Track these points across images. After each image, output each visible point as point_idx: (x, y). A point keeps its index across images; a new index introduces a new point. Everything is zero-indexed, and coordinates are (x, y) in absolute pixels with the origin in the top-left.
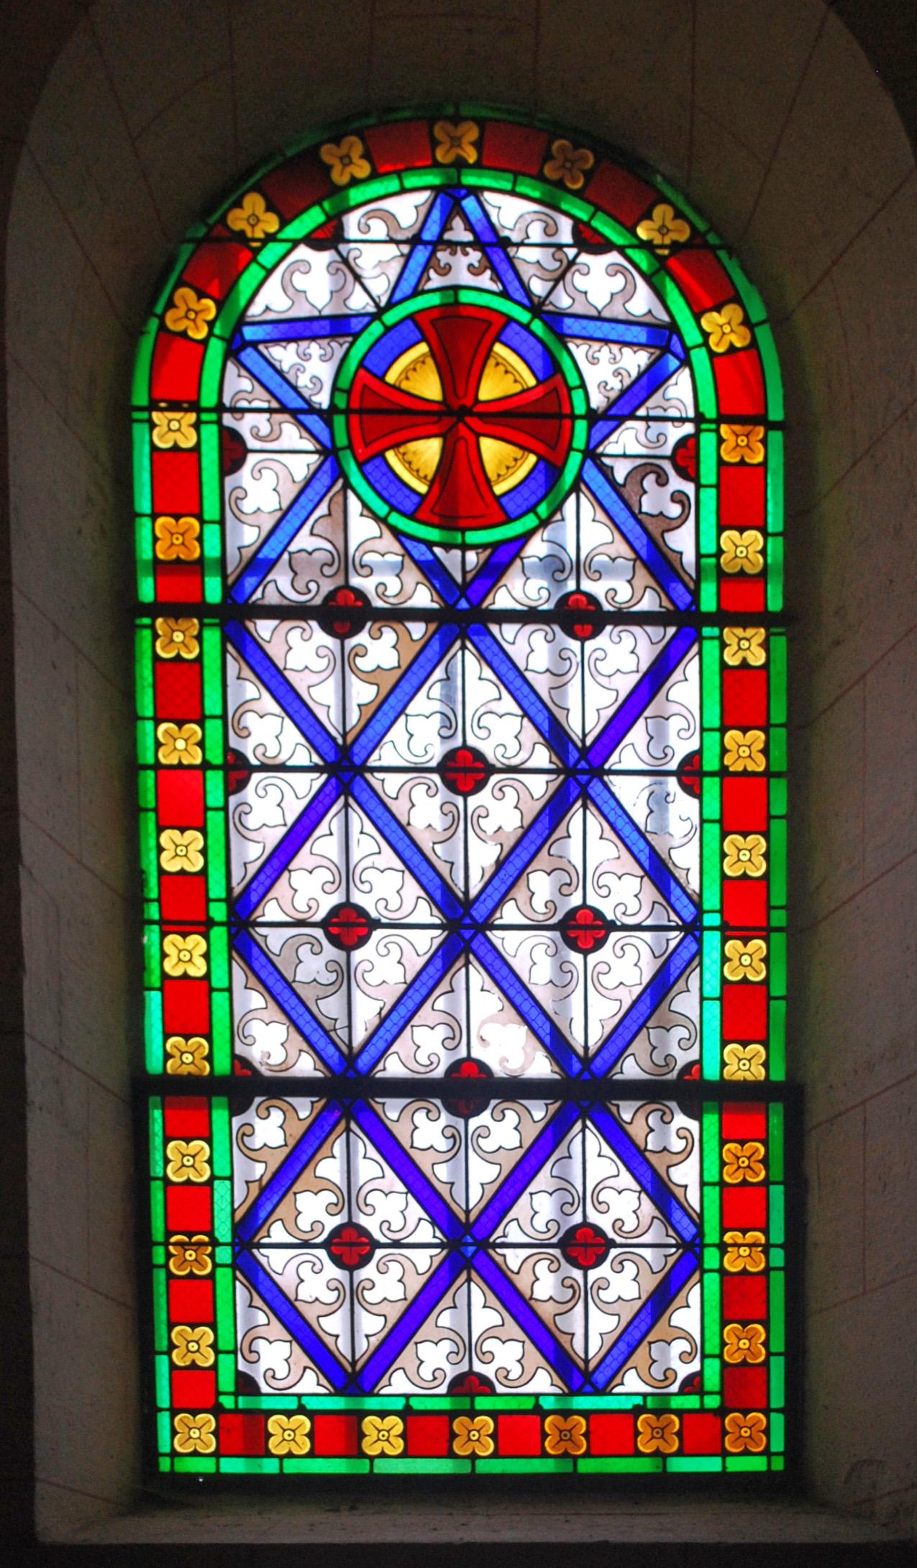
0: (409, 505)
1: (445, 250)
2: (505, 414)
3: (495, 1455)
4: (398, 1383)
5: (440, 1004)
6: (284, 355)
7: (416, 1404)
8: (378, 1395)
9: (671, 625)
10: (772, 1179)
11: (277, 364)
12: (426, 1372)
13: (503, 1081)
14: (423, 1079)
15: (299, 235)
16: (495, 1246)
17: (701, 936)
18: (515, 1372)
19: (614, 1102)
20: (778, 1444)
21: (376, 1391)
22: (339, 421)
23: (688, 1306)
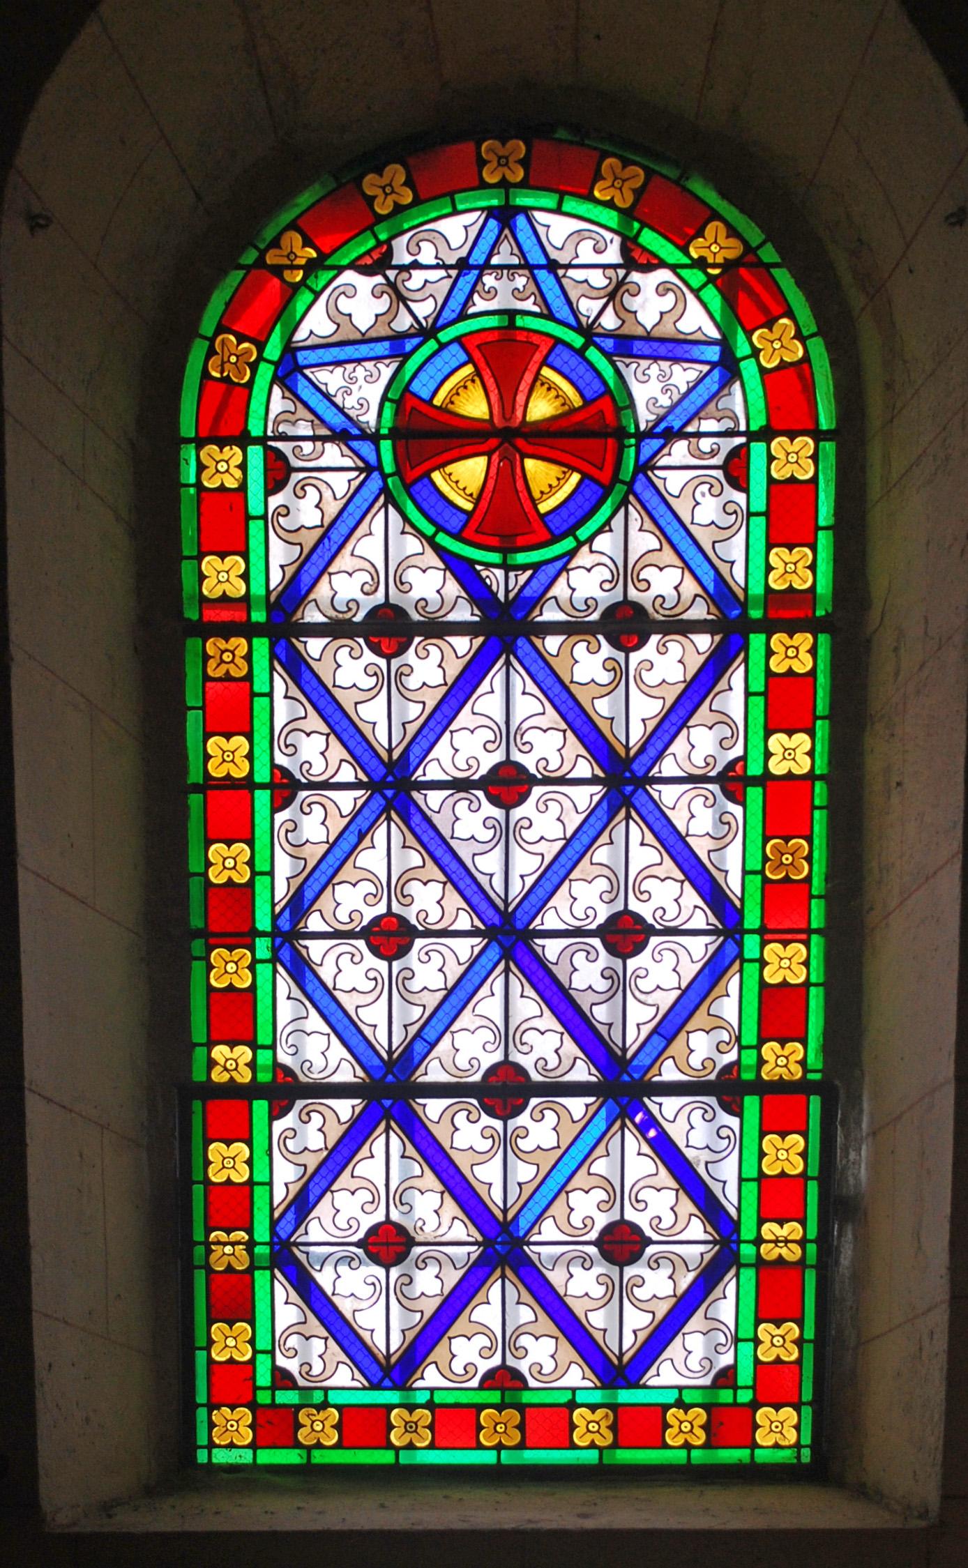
0: (456, 522)
1: (491, 274)
2: (562, 434)
3: (432, 1446)
4: (431, 1377)
5: (417, 1012)
6: (331, 379)
7: (439, 1398)
8: (645, 1387)
9: (717, 634)
10: (256, 1179)
11: (323, 388)
12: (458, 1367)
13: (307, 1085)
14: (465, 1083)
15: (345, 262)
16: (714, 1242)
17: (742, 938)
18: (549, 1366)
19: (419, 1101)
20: (220, 1457)
21: (642, 1382)
22: (386, 446)
23: (488, 1303)
